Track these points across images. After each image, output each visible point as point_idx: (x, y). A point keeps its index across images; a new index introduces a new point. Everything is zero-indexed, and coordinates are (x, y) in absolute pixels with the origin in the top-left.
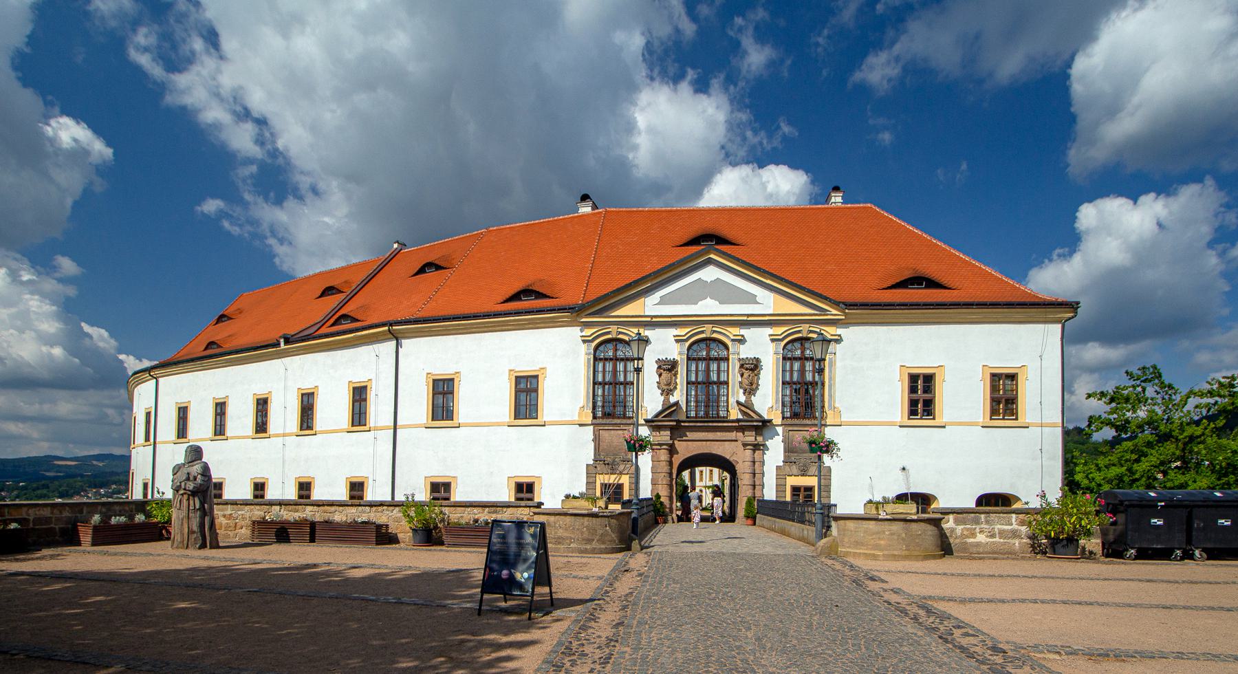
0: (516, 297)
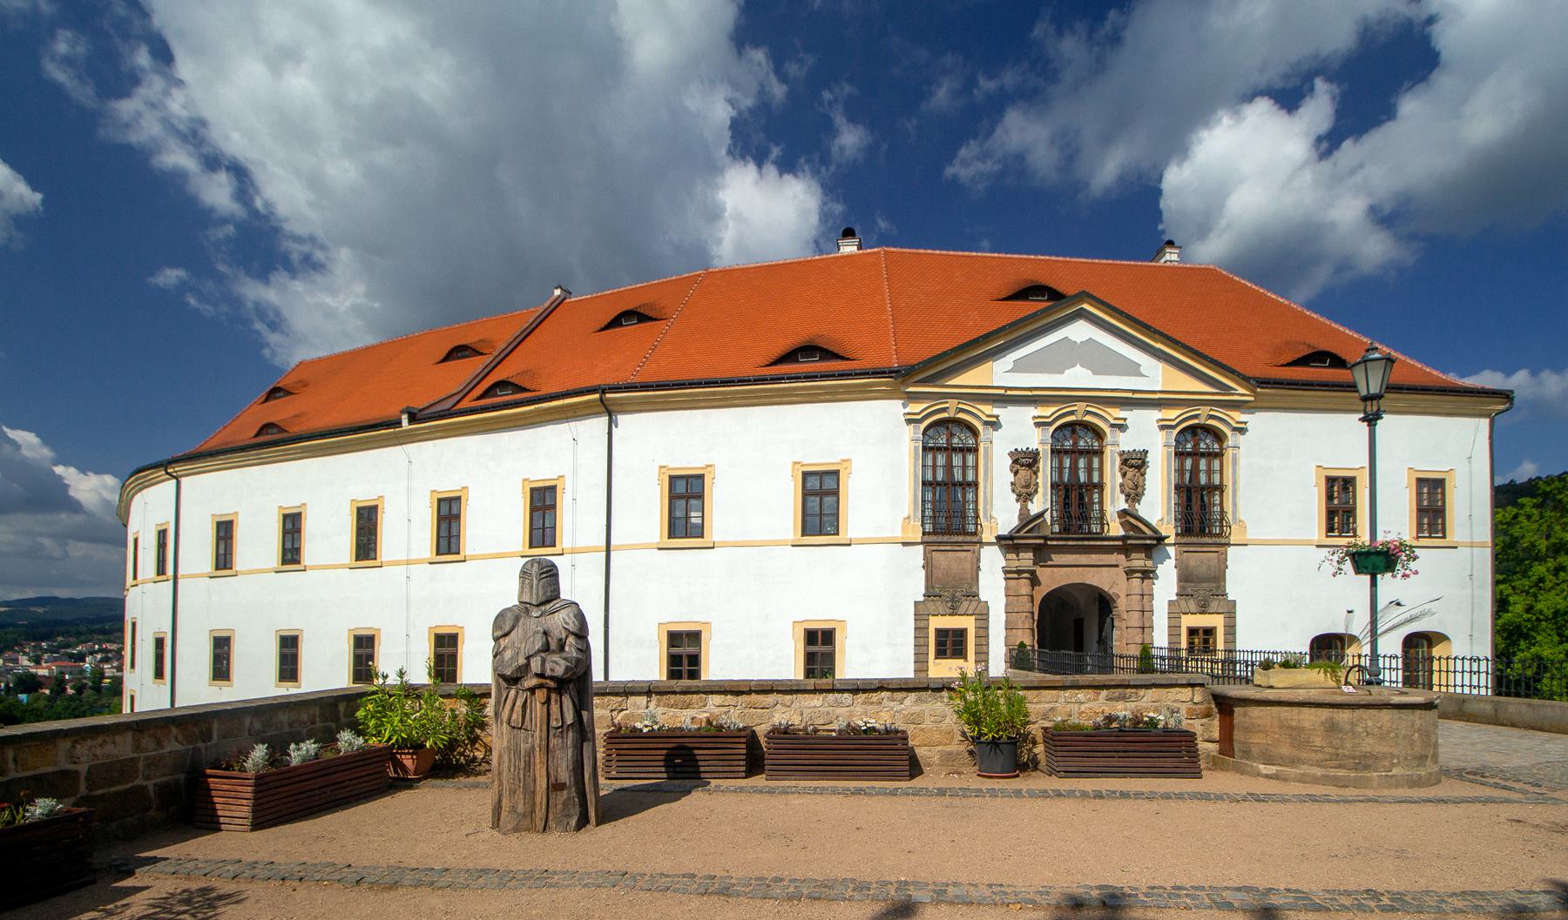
0: (789, 357)
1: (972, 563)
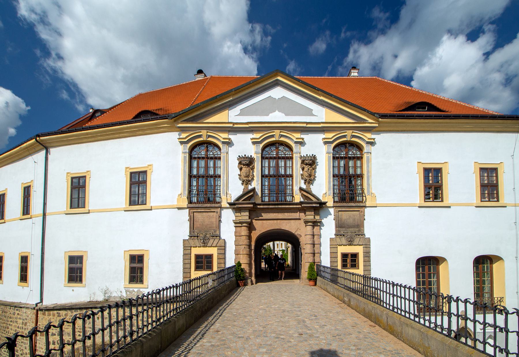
1: (216, 219)
